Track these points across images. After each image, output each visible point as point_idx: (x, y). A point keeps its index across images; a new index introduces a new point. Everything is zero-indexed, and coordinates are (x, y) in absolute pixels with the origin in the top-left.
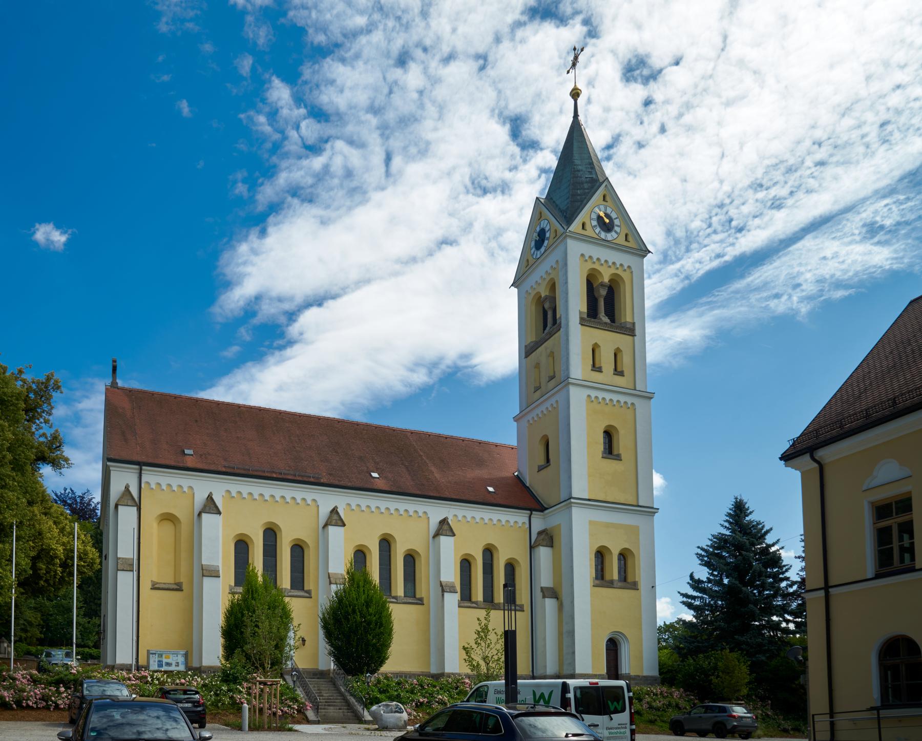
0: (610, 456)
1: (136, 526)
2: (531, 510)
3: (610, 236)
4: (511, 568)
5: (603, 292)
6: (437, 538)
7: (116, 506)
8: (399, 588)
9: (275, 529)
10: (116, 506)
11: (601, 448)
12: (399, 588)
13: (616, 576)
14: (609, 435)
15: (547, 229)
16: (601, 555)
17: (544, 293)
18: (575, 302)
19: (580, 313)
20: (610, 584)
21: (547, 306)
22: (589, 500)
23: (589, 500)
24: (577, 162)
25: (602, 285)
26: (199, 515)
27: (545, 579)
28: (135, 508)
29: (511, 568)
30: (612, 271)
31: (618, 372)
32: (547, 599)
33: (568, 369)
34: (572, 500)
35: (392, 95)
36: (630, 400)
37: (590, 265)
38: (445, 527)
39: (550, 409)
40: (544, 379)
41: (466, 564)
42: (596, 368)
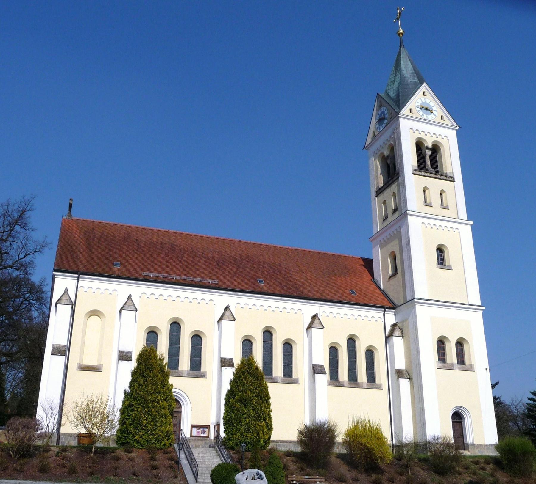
0: (443, 267)
1: (361, 303)
2: (385, 308)
3: (430, 117)
4: (370, 353)
5: (429, 153)
6: (309, 330)
7: (56, 304)
8: (278, 370)
9: (154, 330)
10: (56, 306)
11: (436, 261)
12: (278, 370)
13: (455, 361)
14: (440, 250)
15: (386, 113)
16: (441, 343)
17: (386, 153)
18: (409, 159)
19: (412, 166)
20: (451, 367)
21: (389, 161)
22: (429, 300)
23: (429, 300)
24: (404, 72)
25: (428, 148)
26: (120, 312)
27: (401, 364)
28: (71, 306)
29: (370, 353)
30: (434, 138)
31: (444, 207)
32: (401, 380)
33: (406, 206)
34: (415, 300)
35: (223, 322)
36: (455, 225)
37: (417, 135)
38: (228, 313)
39: (389, 237)
40: (390, 212)
41: (333, 351)
42: (428, 204)
